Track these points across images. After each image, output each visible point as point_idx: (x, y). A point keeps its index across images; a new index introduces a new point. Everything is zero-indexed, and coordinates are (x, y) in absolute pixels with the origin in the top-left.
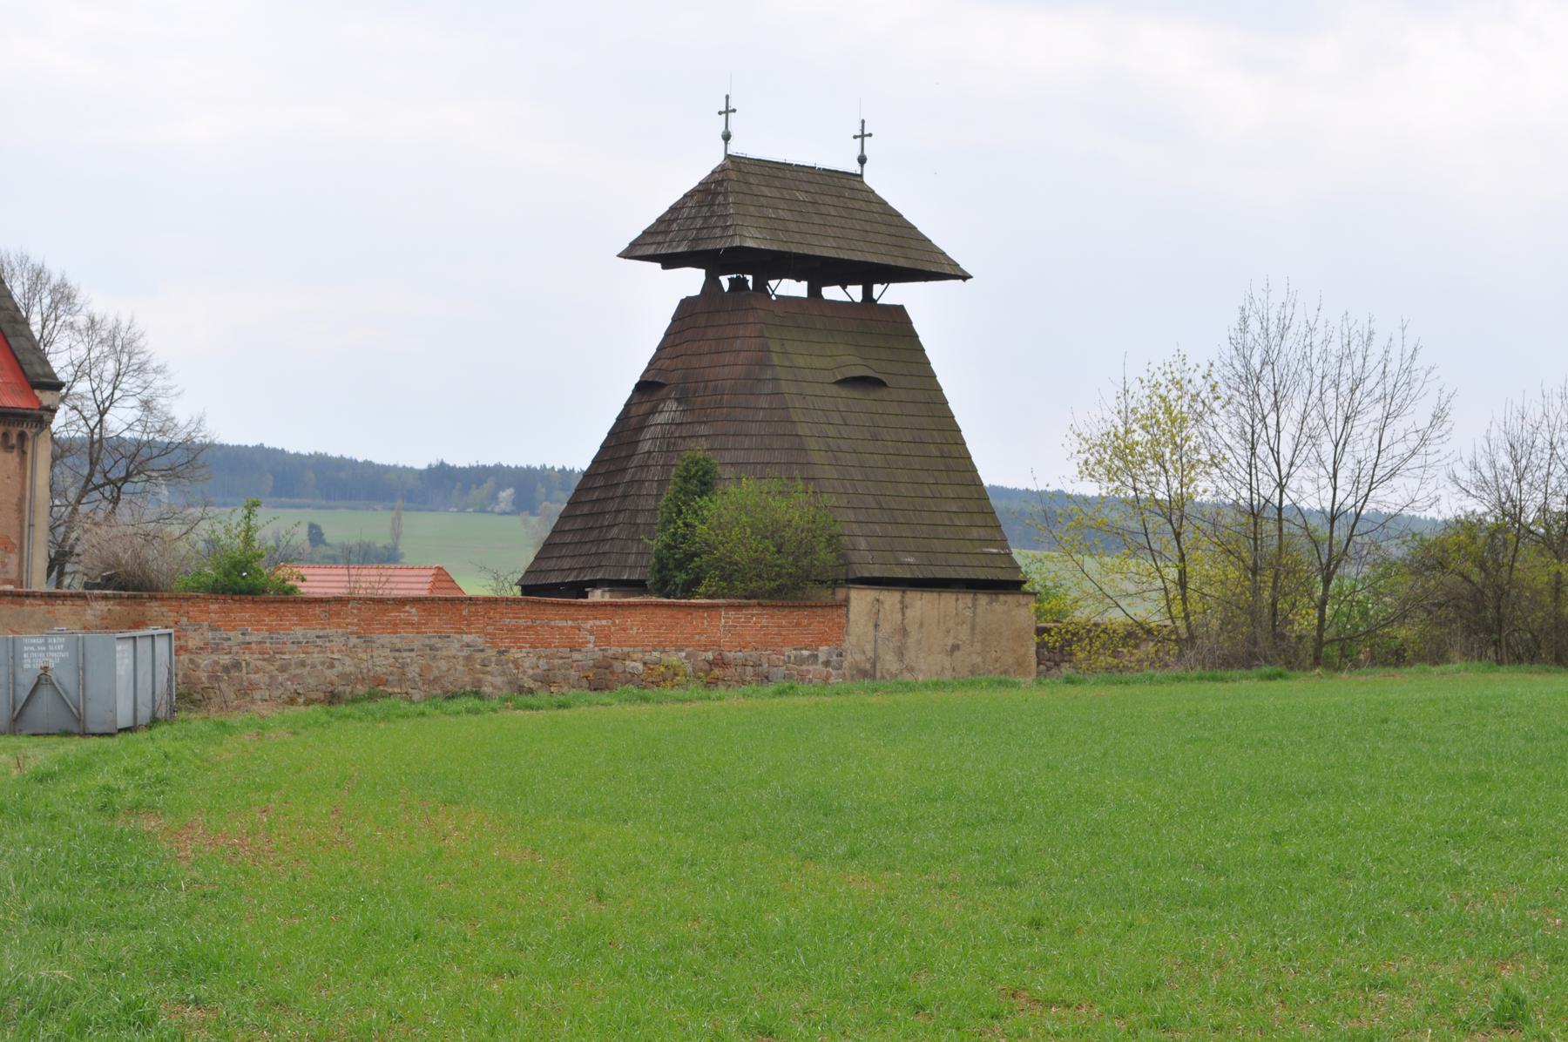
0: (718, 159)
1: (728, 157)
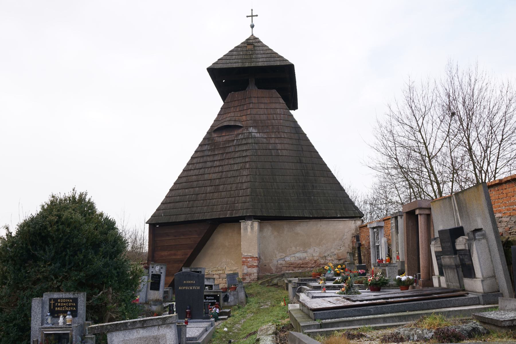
1: (252, 35)
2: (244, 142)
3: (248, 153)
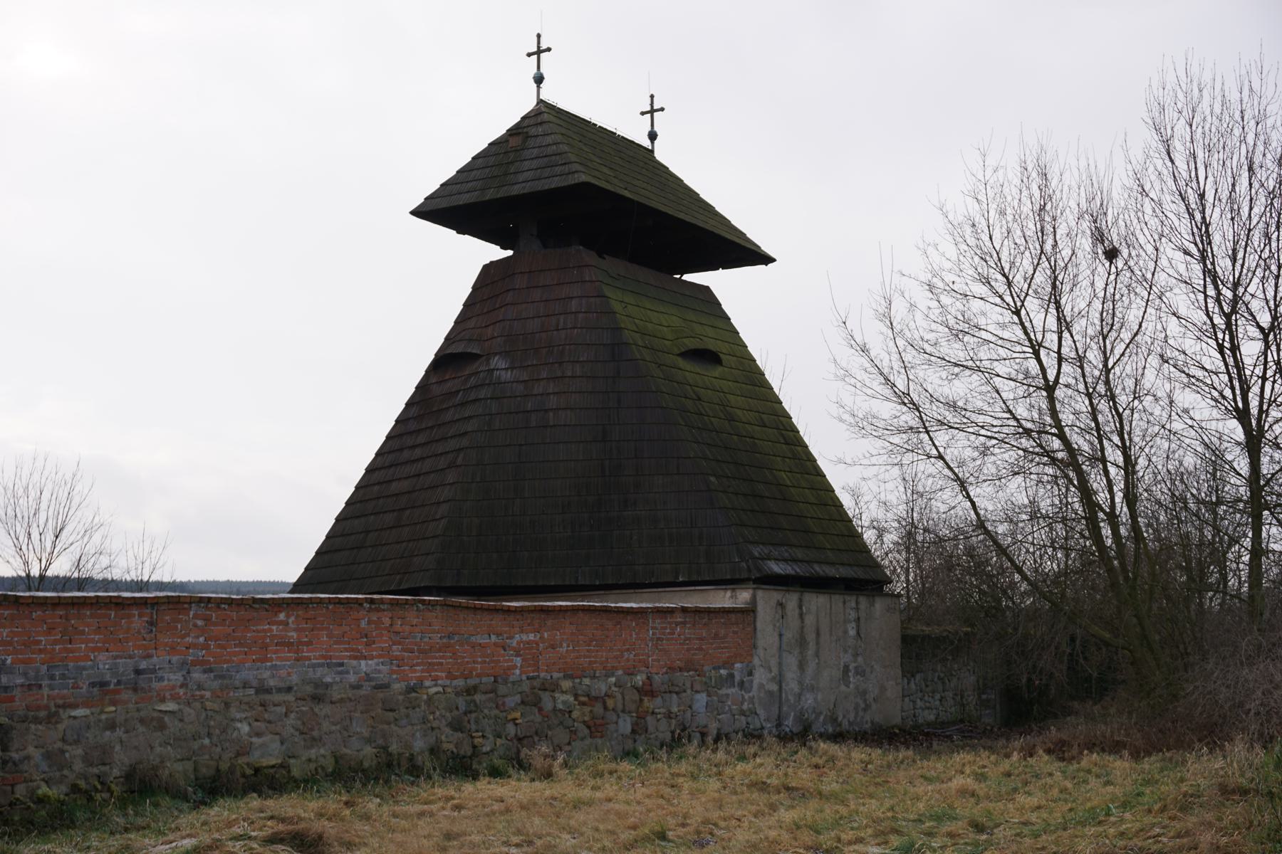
0: (529, 105)
1: (540, 102)
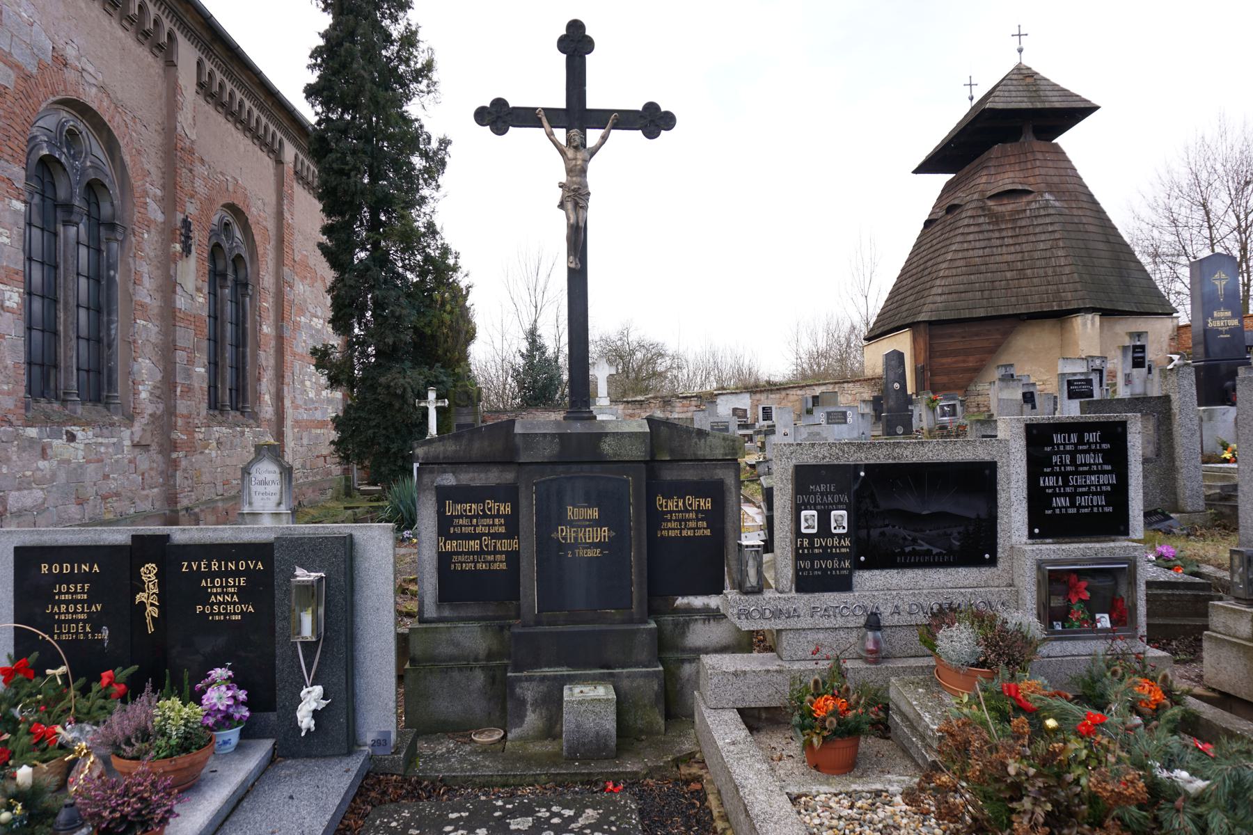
2: (1042, 212)
3: (1056, 227)
